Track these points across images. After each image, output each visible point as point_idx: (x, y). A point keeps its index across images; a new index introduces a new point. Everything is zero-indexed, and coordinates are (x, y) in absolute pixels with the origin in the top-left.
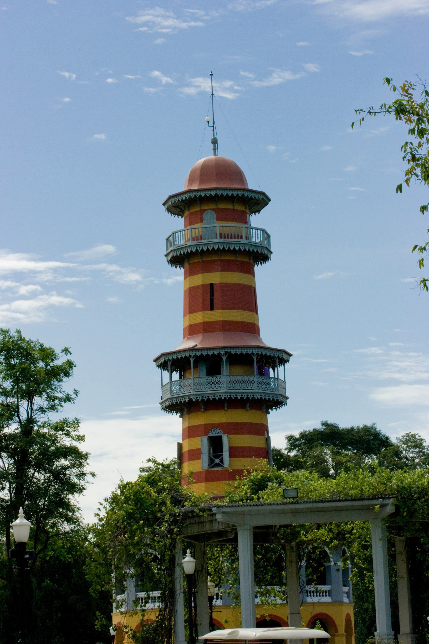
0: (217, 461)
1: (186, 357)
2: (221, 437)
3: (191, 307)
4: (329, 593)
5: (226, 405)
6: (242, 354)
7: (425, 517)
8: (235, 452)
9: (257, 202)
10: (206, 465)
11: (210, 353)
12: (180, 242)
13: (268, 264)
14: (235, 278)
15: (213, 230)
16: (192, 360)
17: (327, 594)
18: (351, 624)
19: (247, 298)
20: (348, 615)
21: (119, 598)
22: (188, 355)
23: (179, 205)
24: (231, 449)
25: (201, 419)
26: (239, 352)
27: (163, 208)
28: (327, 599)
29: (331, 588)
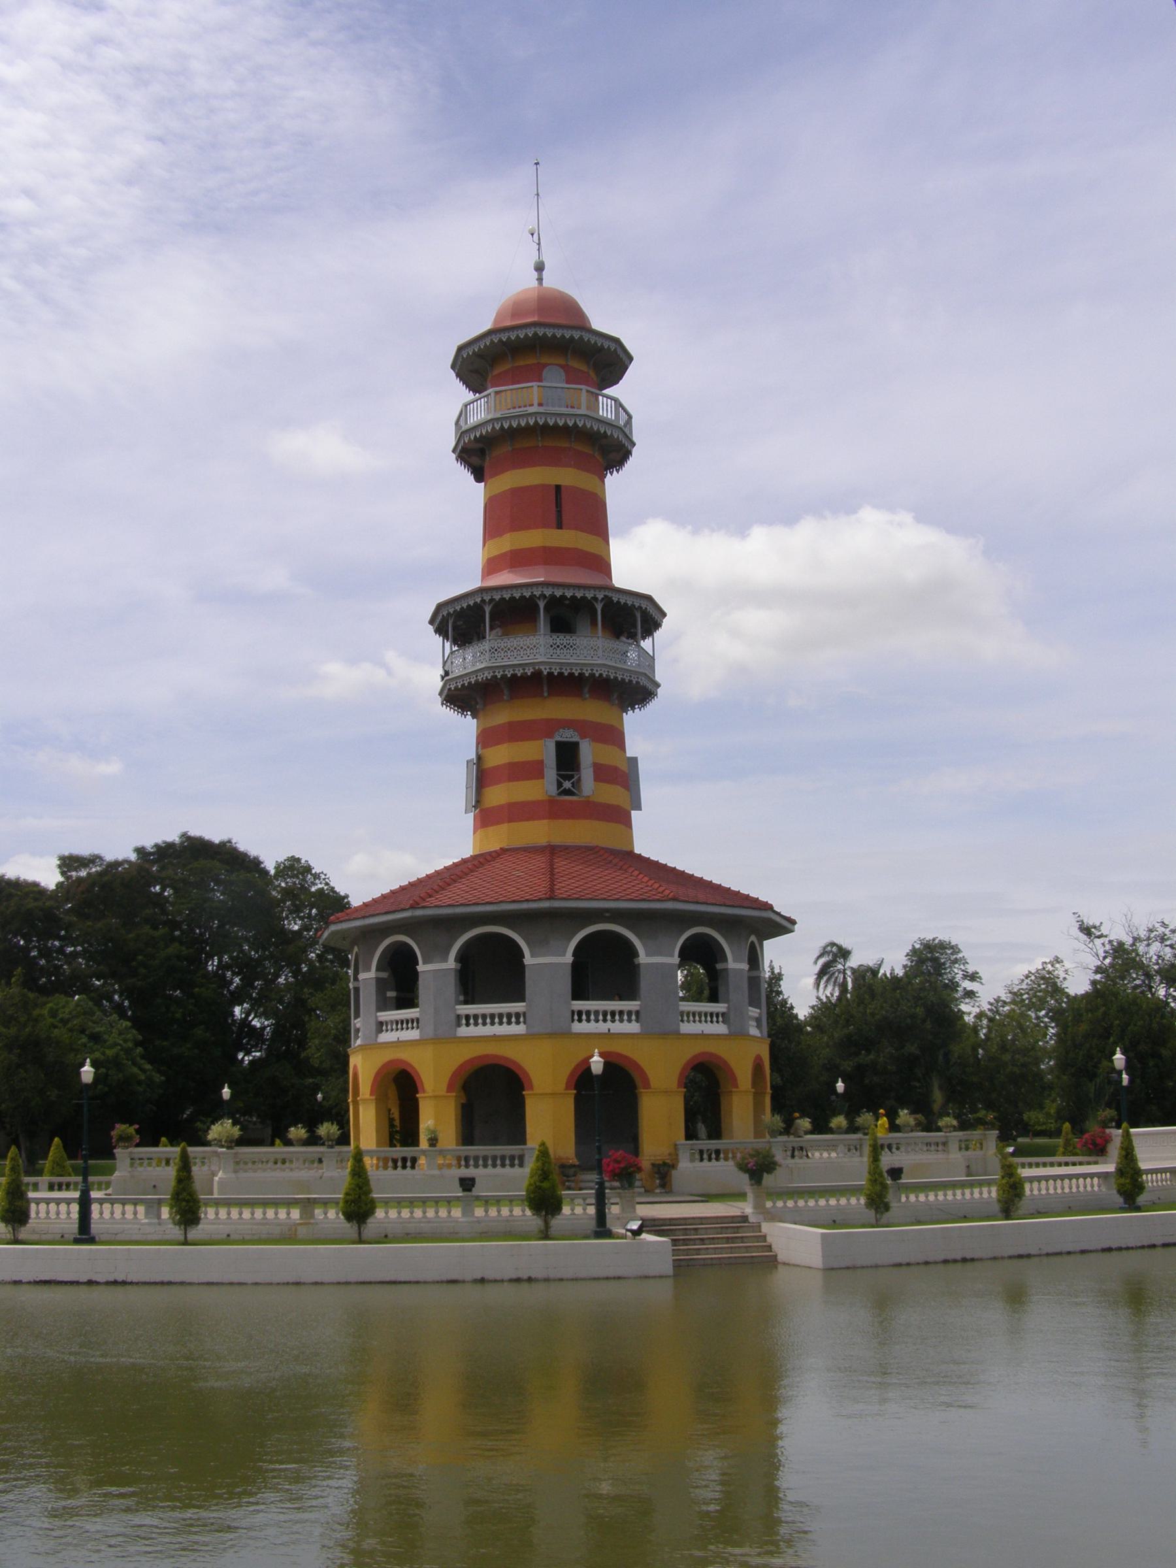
0: (567, 785)
1: (475, 603)
2: (576, 744)
3: (492, 529)
4: (725, 1017)
7: (1052, 997)
8: (532, 770)
10: (553, 789)
11: (569, 594)
14: (567, 476)
15: (539, 397)
16: (488, 609)
17: (720, 1019)
18: (765, 1078)
19: (595, 520)
22: (478, 600)
23: (478, 364)
25: (502, 716)
26: (507, 596)
27: (431, 628)
28: (633, 1027)
29: (728, 1008)
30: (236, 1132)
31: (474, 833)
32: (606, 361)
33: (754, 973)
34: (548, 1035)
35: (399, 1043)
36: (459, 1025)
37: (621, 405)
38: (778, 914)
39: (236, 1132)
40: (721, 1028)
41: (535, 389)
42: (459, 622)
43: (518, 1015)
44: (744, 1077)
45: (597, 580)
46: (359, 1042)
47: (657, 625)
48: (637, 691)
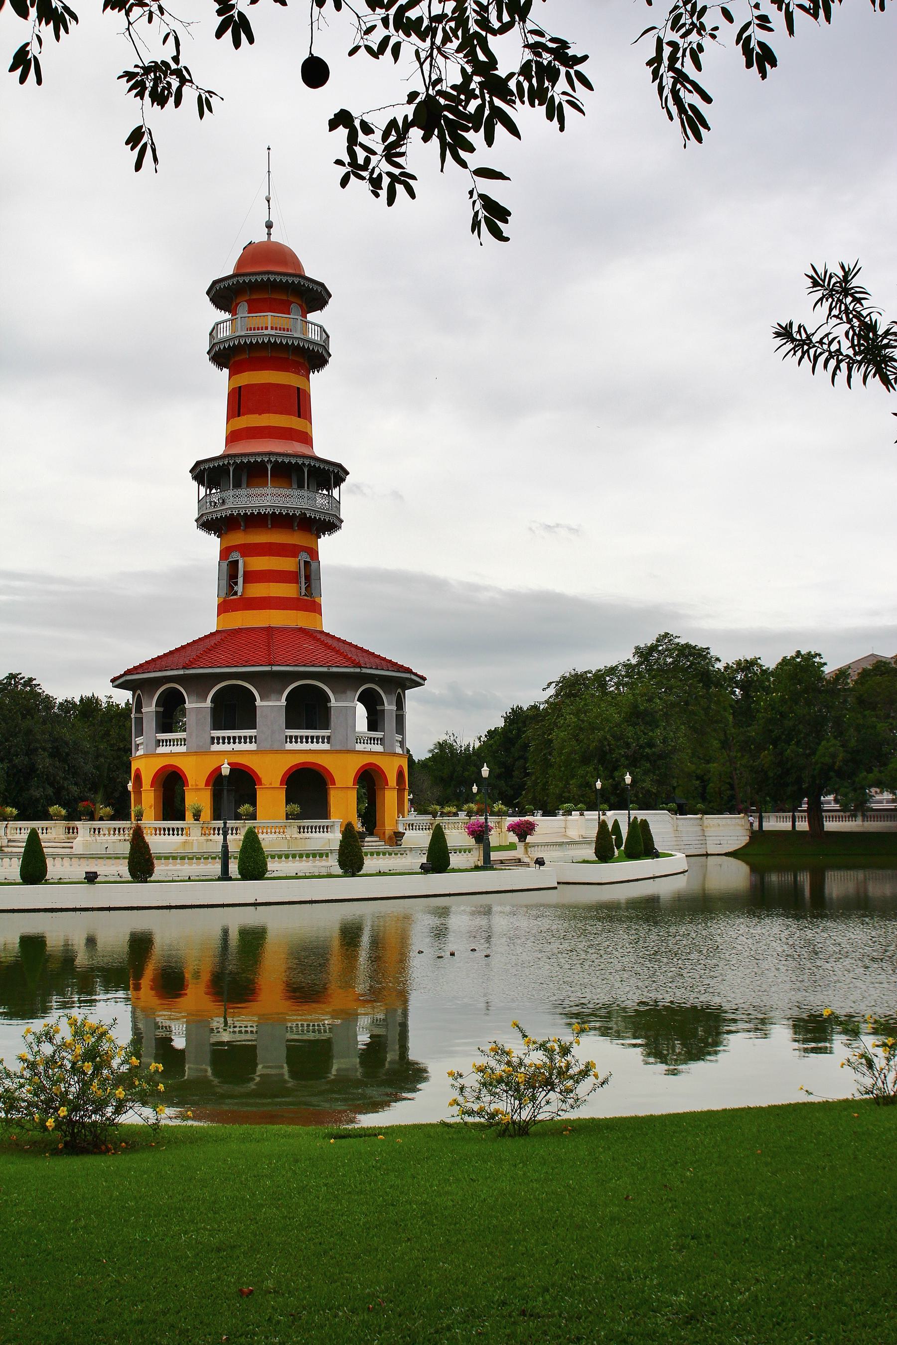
1: (224, 464)
4: (382, 741)
5: (269, 522)
6: (290, 463)
8: (251, 577)
9: (315, 296)
12: (225, 333)
13: (337, 535)
15: (268, 325)
19: (299, 404)
20: (401, 767)
21: (139, 740)
23: (223, 294)
24: (246, 573)
25: (239, 538)
30: (112, 813)
31: (218, 616)
32: (315, 296)
33: (400, 713)
34: (270, 746)
35: (171, 754)
36: (213, 743)
37: (324, 331)
38: (416, 674)
39: (112, 813)
40: (379, 748)
41: (270, 318)
42: (207, 473)
43: (251, 737)
44: (392, 780)
45: (298, 448)
46: (138, 753)
47: (343, 480)
48: (331, 525)
